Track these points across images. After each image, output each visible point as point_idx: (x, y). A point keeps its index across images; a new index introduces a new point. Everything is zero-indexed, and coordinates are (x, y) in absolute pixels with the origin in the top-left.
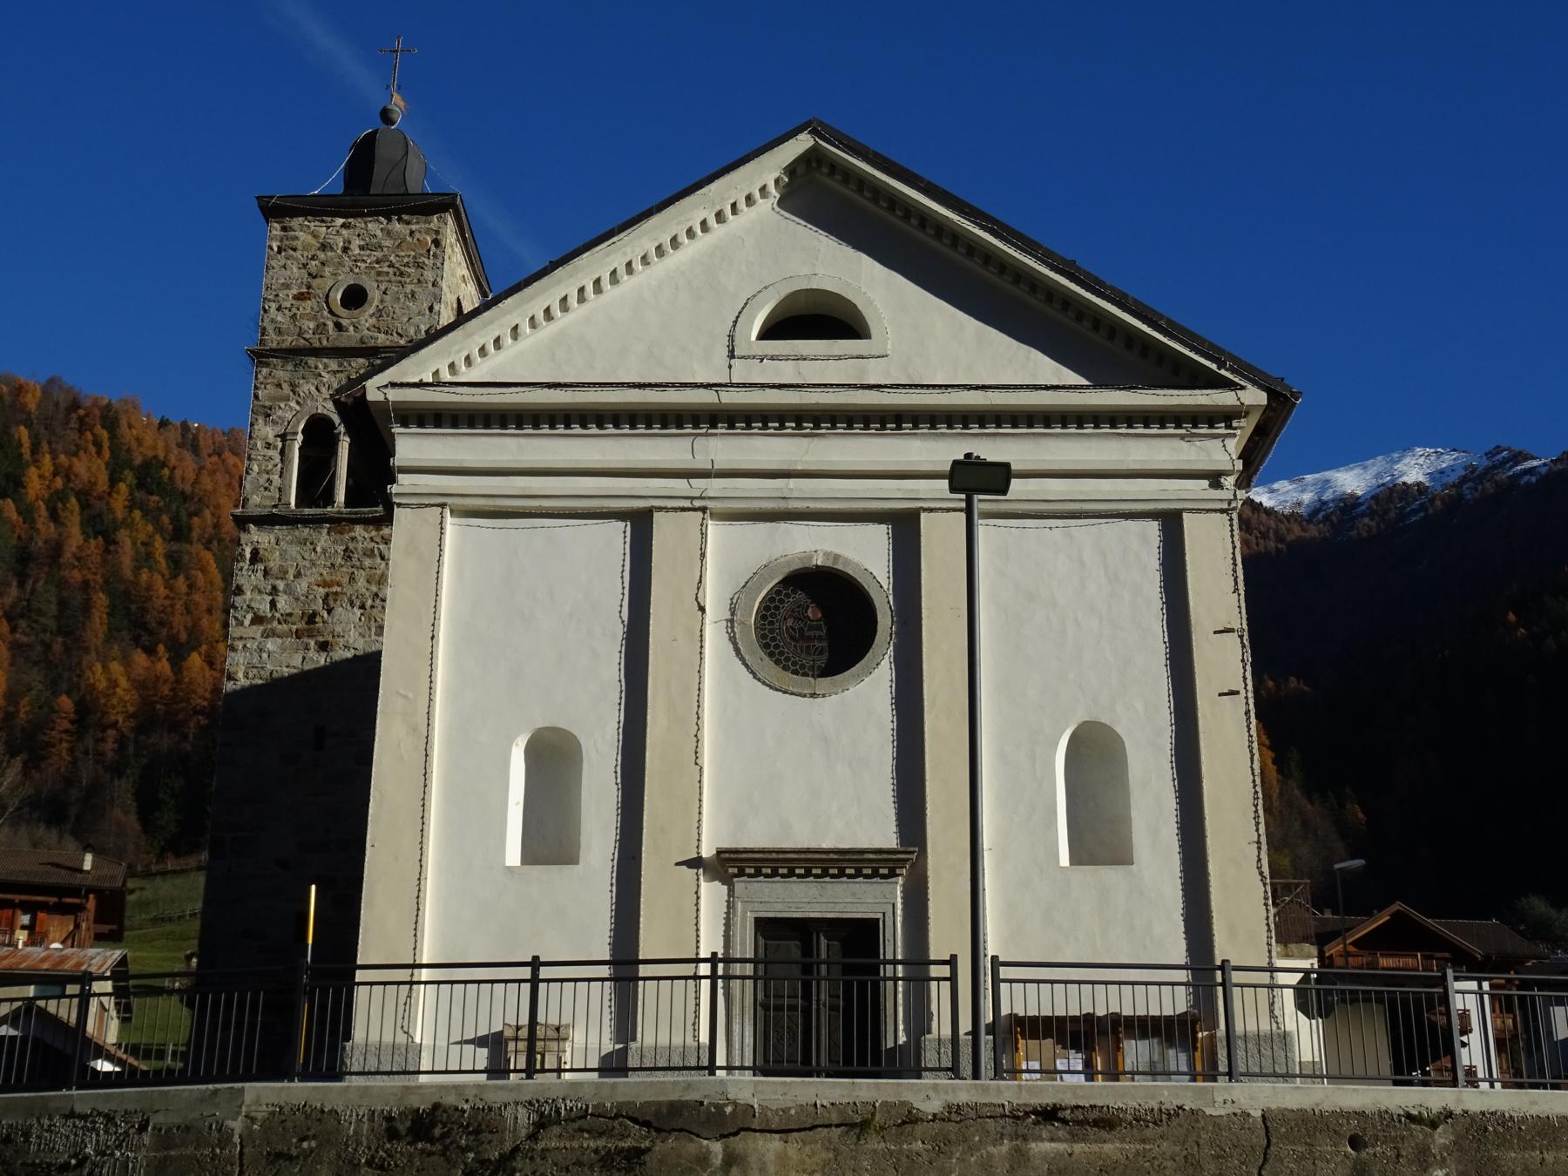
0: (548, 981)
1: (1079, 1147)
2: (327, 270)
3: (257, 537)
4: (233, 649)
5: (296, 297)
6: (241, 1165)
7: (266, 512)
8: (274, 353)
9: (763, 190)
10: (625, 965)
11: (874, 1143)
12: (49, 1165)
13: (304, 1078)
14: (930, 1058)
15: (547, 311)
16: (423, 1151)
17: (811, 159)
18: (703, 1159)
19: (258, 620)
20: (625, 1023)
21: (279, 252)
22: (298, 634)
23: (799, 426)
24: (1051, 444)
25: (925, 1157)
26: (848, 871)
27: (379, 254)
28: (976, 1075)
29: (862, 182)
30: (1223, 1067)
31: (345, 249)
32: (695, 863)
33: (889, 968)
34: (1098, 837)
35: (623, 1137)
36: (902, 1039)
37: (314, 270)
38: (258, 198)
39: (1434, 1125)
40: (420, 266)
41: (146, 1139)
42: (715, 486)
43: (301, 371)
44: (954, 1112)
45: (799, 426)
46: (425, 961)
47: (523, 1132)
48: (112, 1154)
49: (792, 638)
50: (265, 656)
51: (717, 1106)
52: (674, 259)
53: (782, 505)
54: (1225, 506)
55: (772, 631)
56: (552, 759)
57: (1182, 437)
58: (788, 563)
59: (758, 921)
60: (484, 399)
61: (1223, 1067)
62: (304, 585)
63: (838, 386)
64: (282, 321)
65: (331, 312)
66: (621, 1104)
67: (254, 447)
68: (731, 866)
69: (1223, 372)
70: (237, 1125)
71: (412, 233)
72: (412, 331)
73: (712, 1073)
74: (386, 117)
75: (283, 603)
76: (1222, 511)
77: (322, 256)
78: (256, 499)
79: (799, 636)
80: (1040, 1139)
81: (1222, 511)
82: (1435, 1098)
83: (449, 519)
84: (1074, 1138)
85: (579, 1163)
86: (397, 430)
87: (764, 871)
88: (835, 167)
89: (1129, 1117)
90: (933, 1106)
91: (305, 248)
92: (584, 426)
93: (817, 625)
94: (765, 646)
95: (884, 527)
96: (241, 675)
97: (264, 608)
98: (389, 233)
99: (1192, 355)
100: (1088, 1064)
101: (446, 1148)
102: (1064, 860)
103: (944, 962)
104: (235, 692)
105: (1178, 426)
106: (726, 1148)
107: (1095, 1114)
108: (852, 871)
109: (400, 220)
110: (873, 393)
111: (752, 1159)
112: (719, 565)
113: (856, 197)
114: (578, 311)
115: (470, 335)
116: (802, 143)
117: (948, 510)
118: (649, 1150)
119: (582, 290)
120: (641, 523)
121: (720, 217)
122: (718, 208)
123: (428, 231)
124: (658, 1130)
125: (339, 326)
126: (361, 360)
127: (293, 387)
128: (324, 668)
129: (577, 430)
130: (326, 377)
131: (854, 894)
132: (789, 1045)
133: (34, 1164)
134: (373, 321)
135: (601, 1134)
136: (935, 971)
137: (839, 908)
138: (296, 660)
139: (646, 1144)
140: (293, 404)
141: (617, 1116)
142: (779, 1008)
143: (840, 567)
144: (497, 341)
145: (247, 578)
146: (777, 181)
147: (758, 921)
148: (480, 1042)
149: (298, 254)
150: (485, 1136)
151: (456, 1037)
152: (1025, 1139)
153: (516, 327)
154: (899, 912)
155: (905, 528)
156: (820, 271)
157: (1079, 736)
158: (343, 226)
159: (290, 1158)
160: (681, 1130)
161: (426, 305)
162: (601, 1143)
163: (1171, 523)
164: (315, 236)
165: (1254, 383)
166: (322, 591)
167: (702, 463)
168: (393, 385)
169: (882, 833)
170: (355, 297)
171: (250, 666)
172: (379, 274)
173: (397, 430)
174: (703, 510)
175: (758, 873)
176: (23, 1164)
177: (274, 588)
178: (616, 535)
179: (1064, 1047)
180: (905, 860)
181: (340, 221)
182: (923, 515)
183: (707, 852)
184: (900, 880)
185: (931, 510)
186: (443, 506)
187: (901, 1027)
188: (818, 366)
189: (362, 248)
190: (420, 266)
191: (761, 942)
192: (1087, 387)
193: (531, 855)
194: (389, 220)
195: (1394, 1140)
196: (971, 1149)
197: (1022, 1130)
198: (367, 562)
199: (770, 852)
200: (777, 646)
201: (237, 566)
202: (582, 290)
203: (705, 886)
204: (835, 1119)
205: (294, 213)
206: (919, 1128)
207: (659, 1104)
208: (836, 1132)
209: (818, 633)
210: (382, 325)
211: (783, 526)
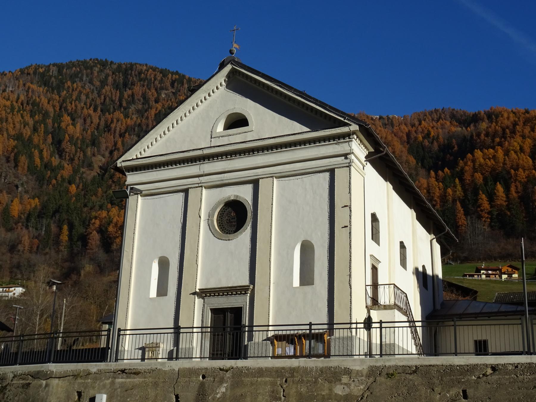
1: (128, 380)
11: (80, 381)
13: (53, 363)
17: (233, 72)
18: (41, 386)
20: (176, 343)
23: (227, 157)
25: (90, 384)
30: (174, 356)
32: (194, 293)
39: (227, 371)
44: (100, 372)
45: (227, 157)
46: (128, 328)
52: (198, 110)
54: (348, 165)
56: (307, 250)
57: (336, 144)
58: (224, 200)
61: (174, 356)
63: (253, 140)
68: (204, 293)
69: (345, 121)
76: (347, 167)
79: (229, 222)
80: (119, 378)
81: (347, 167)
82: (240, 363)
83: (275, 179)
84: (127, 378)
89: (143, 371)
93: (234, 217)
105: (334, 141)
106: (46, 382)
107: (134, 371)
112: (207, 202)
115: (142, 143)
116: (229, 68)
117: (267, 177)
120: (332, 172)
136: (103, 333)
137: (232, 304)
142: (218, 335)
143: (238, 199)
146: (225, 81)
148: (140, 349)
151: (137, 347)
152: (115, 378)
156: (236, 107)
165: (355, 123)
168: (123, 161)
169: (245, 281)
174: (202, 186)
178: (181, 195)
185: (262, 178)
188: (238, 137)
192: (309, 132)
195: (214, 376)
197: (115, 376)
206: (90, 376)
211: (224, 188)
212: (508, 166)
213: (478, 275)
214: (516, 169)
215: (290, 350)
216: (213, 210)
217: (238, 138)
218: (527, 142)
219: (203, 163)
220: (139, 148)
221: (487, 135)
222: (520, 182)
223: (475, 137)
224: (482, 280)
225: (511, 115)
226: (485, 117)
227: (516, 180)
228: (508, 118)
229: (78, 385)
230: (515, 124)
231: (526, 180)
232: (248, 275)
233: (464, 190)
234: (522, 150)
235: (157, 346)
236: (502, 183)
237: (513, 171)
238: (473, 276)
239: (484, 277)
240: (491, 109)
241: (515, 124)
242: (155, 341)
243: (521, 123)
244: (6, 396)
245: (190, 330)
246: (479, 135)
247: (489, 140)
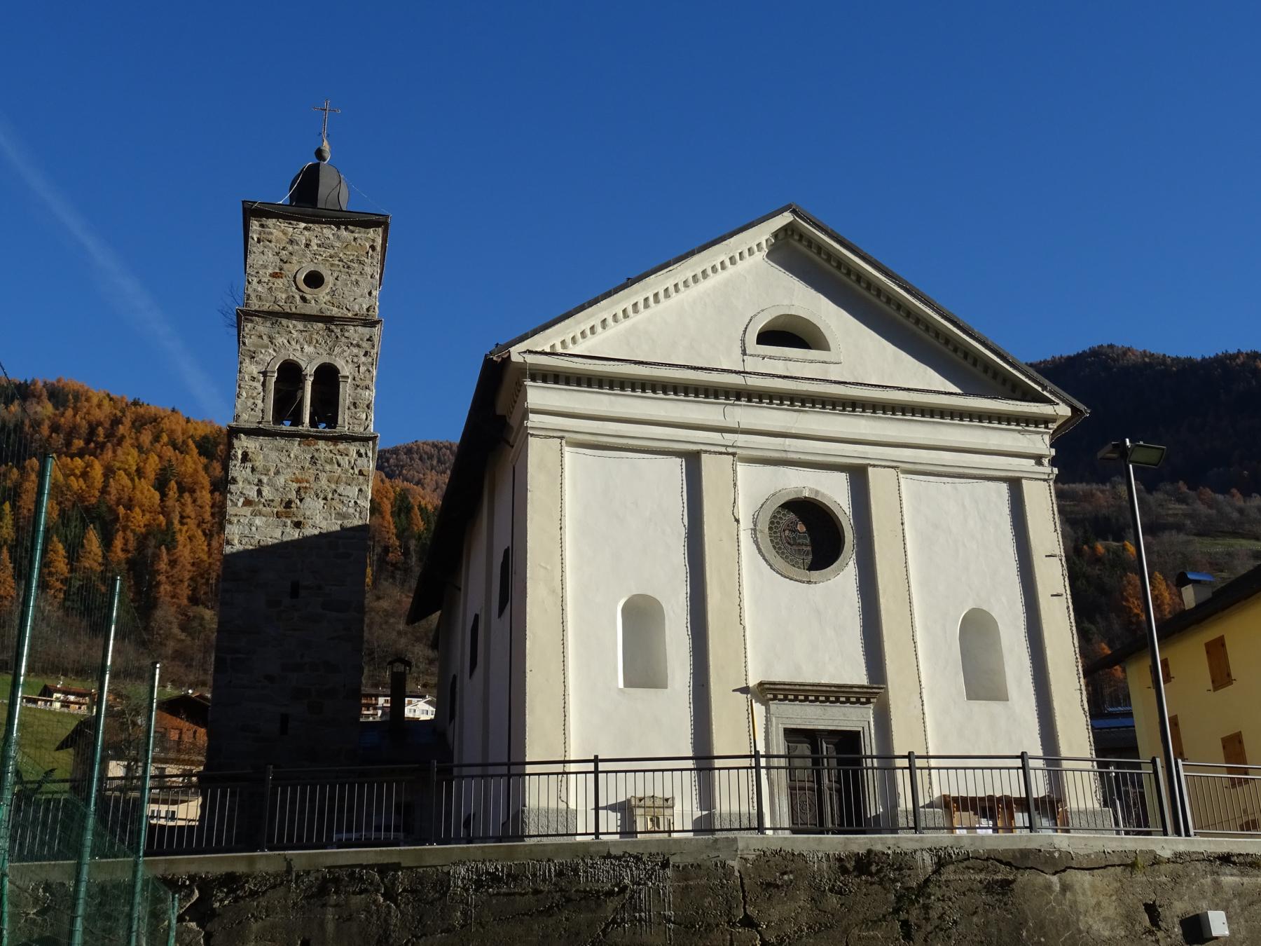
0: (719, 769)
1: (1246, 880)
2: (294, 259)
3: (244, 444)
4: (230, 523)
5: (271, 275)
6: (744, 892)
7: (254, 426)
8: (257, 313)
10: (703, 761)
12: (597, 892)
14: (902, 822)
15: (624, 311)
16: (867, 882)
17: (788, 229)
18: (1048, 887)
19: (248, 503)
20: (706, 795)
21: (259, 241)
22: (278, 515)
23: (792, 404)
24: (969, 432)
27: (331, 251)
28: (1187, 834)
29: (820, 248)
31: (307, 245)
32: (745, 690)
33: (869, 761)
34: (982, 682)
35: (996, 873)
37: (285, 258)
38: (244, 202)
40: (361, 263)
41: (669, 872)
42: (741, 439)
43: (277, 328)
44: (1178, 857)
45: (792, 404)
47: (930, 870)
48: (645, 884)
50: (254, 529)
51: (1049, 852)
52: (704, 285)
53: (783, 455)
57: (1019, 432)
59: (786, 730)
62: (282, 480)
64: (261, 293)
65: (298, 288)
66: (989, 851)
67: (243, 379)
68: (769, 692)
70: (735, 864)
71: (355, 239)
72: (357, 308)
73: (763, 833)
74: (319, 154)
75: (266, 491)
76: (1045, 480)
77: (290, 248)
78: (245, 416)
80: (1225, 874)
81: (1045, 480)
84: (1242, 874)
85: (971, 890)
86: (528, 383)
88: (802, 236)
90: (1167, 854)
91: (277, 241)
92: (654, 392)
93: (810, 536)
96: (236, 542)
97: (252, 494)
98: (338, 237)
99: (1026, 380)
100: (995, 824)
101: (881, 880)
103: (904, 757)
104: (233, 554)
106: (1060, 879)
107: (1249, 859)
109: (346, 229)
110: (841, 387)
111: (1077, 887)
112: (745, 495)
113: (816, 258)
114: (644, 314)
116: (786, 218)
117: (885, 467)
118: (1014, 881)
119: (646, 300)
120: (692, 461)
121: (732, 260)
123: (367, 239)
124: (1017, 868)
125: (304, 299)
126: (321, 325)
127: (271, 339)
128: (298, 540)
129: (650, 394)
130: (295, 334)
133: (585, 891)
134: (328, 298)
135: (981, 871)
137: (836, 723)
138: (278, 534)
139: (1011, 877)
140: (271, 351)
141: (987, 859)
143: (819, 498)
144: (592, 328)
145: (238, 471)
147: (786, 730)
149: (272, 245)
150: (906, 872)
155: (858, 476)
156: (796, 304)
157: (960, 617)
158: (305, 228)
159: (777, 886)
160: (1031, 868)
161: (366, 291)
162: (982, 876)
163: (1015, 485)
164: (285, 234)
165: (1064, 401)
166: (295, 485)
167: (731, 423)
168: (530, 352)
169: (857, 675)
170: (315, 280)
171: (243, 536)
172: (332, 265)
173: (528, 383)
174: (734, 454)
175: (786, 698)
176: (577, 891)
177: (260, 481)
178: (676, 467)
180: (873, 693)
181: (303, 225)
182: (870, 469)
183: (752, 683)
185: (874, 466)
189: (319, 246)
190: (361, 263)
194: (339, 228)
196: (1192, 881)
197: (1215, 869)
198: (328, 467)
201: (232, 463)
202: (646, 300)
204: (1116, 861)
205: (269, 215)
206: (1163, 867)
207: (1014, 851)
208: (1119, 869)
210: (335, 301)
212: (113, 497)
213: (46, 701)
214: (129, 507)
217: (779, 368)
218: (151, 460)
219: (733, 405)
221: (55, 428)
222: (132, 531)
223: (26, 428)
224: (54, 713)
225: (106, 402)
226: (45, 393)
227: (125, 528)
228: (99, 406)
229: (1141, 887)
230: (116, 422)
231: (143, 530)
233: (17, 527)
234: (140, 472)
235: (668, 803)
236: (98, 526)
237: (121, 510)
238: (35, 701)
239: (57, 705)
240: (59, 381)
241: (116, 422)
242: (659, 794)
243: (127, 422)
244: (934, 914)
245: (559, 768)
246: (36, 424)
247: (58, 440)
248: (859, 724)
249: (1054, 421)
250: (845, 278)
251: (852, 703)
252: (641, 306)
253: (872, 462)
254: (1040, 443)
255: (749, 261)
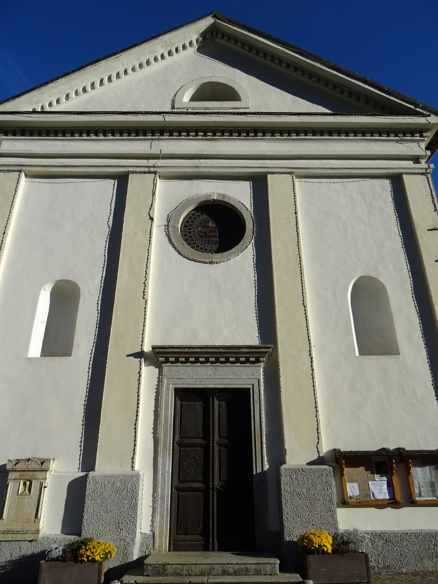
9: (191, 43)
23: (205, 135)
26: (231, 359)
32: (140, 355)
36: (266, 467)
45: (205, 135)
49: (200, 236)
52: (147, 70)
54: (424, 171)
55: (190, 233)
56: (64, 297)
57: (397, 141)
58: (199, 198)
60: (45, 119)
68: (161, 356)
69: (417, 109)
76: (422, 174)
87: (181, 359)
93: (214, 229)
94: (186, 240)
95: (248, 183)
99: (401, 102)
102: (357, 354)
105: (396, 136)
108: (234, 359)
112: (162, 200)
116: (208, 21)
117: (281, 173)
120: (122, 180)
121: (170, 53)
122: (169, 49)
131: (234, 373)
132: (167, 498)
137: (226, 382)
143: (226, 200)
146: (197, 41)
153: (68, 94)
154: (262, 384)
169: (250, 337)
174: (155, 173)
175: (177, 361)
178: (109, 187)
179: (372, 473)
180: (265, 352)
182: (269, 176)
184: (262, 365)
186: (20, 171)
187: (266, 458)
191: (179, 402)
193: (48, 350)
199: (184, 348)
200: (192, 240)
203: (144, 369)
209: (214, 234)
211: (196, 182)
215: (379, 488)
216: (178, 210)
219: (158, 139)
220: (35, 99)
232: (257, 329)
248: (248, 381)
249: (427, 130)
250: (256, 57)
251: (242, 363)
252: (97, 84)
253: (270, 170)
254: (418, 148)
255: (183, 54)
